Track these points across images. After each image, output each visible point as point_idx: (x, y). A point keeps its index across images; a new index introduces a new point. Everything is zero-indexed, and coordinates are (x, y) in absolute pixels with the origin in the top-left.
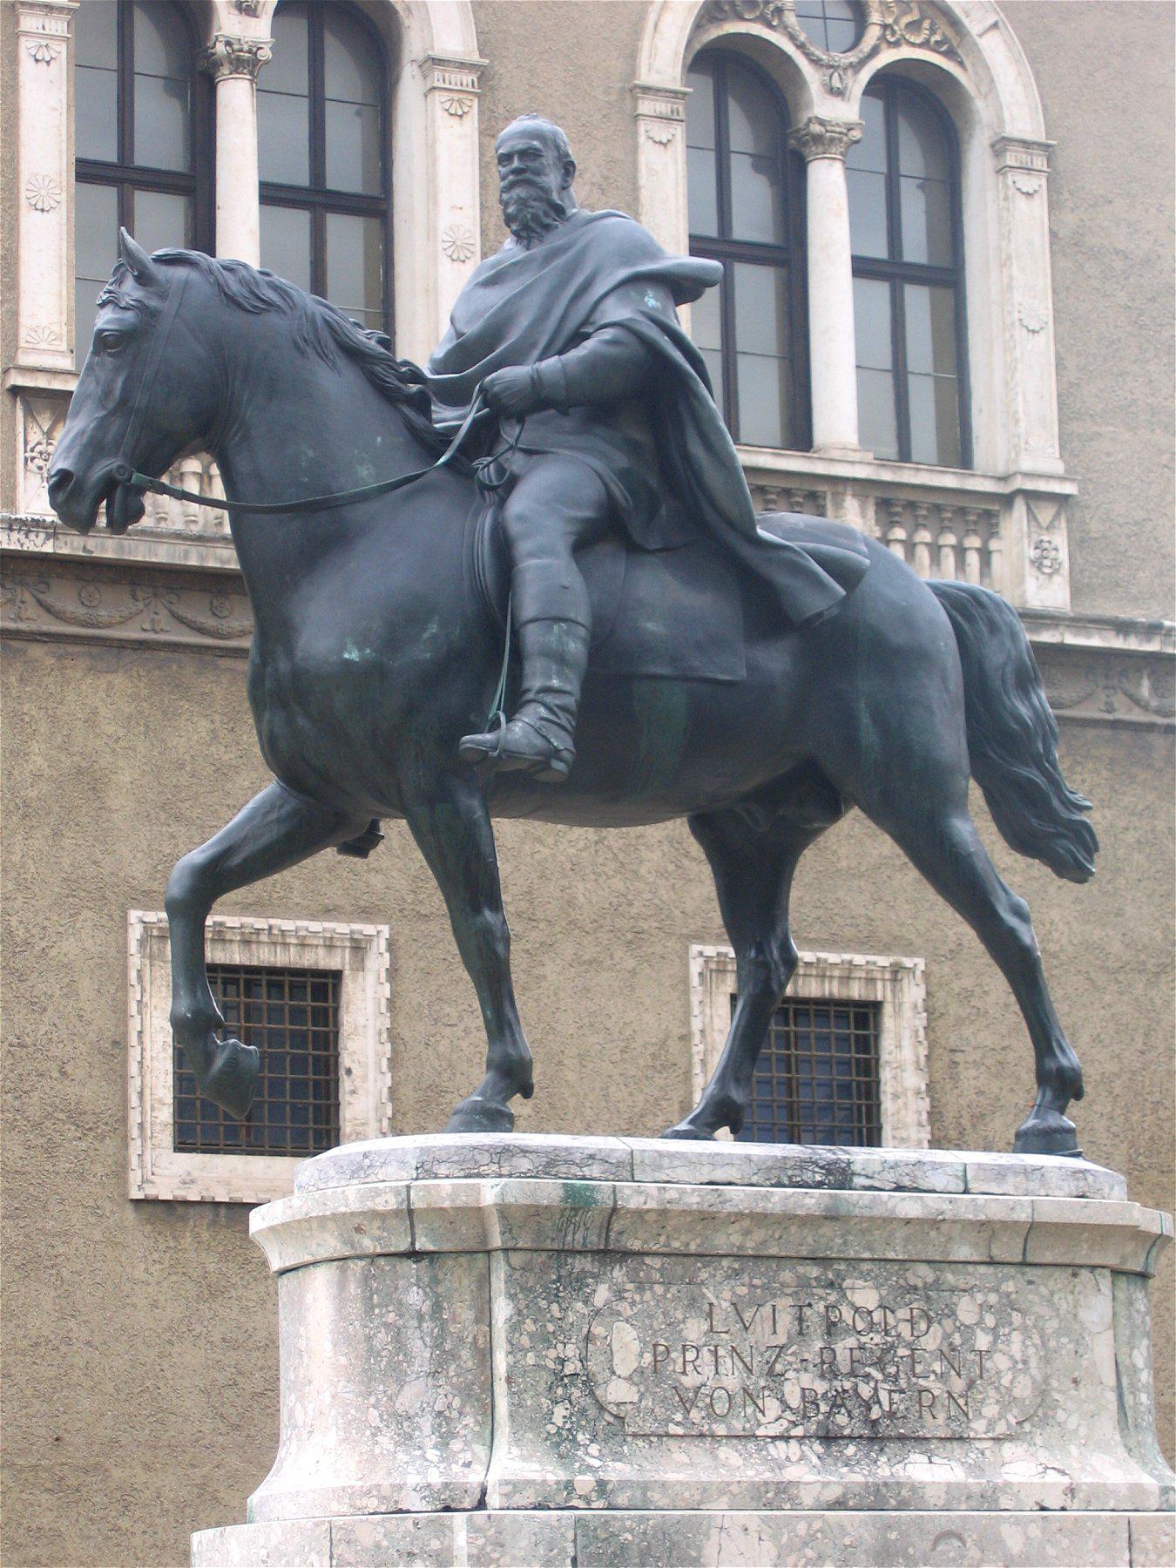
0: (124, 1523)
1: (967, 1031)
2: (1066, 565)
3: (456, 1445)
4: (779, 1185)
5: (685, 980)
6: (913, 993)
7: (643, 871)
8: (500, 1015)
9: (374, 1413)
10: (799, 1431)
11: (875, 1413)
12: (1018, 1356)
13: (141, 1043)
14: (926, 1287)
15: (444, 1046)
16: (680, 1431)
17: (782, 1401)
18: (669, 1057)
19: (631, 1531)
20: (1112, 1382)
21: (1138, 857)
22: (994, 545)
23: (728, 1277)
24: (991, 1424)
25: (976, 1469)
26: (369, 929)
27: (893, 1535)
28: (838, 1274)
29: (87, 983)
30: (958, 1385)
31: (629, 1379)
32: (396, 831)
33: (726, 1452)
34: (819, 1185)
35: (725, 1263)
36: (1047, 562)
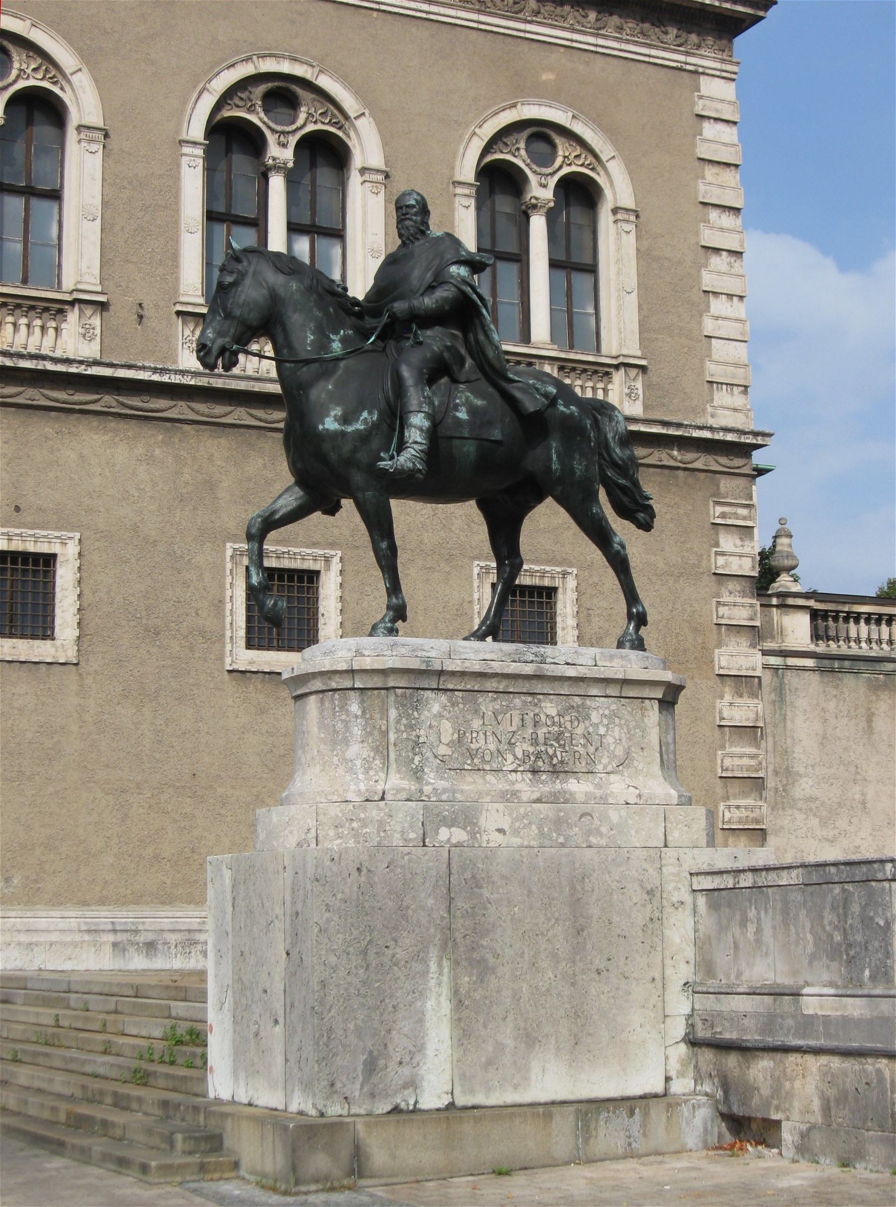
0: (223, 812)
1: (595, 601)
2: (641, 396)
3: (372, 773)
4: (514, 661)
5: (471, 577)
6: (571, 583)
7: (453, 528)
8: (394, 588)
9: (336, 759)
10: (521, 769)
11: (555, 761)
12: (617, 737)
13: (231, 601)
14: (578, 706)
15: (365, 604)
16: (470, 768)
17: (514, 755)
18: (462, 612)
19: (448, 811)
20: (658, 749)
21: (671, 525)
22: (610, 387)
23: (491, 701)
24: (605, 767)
25: (598, 786)
26: (333, 553)
27: (562, 814)
28: (539, 700)
29: (208, 574)
30: (591, 749)
31: (447, 745)
32: (347, 504)
33: (490, 777)
34: (532, 661)
35: (490, 694)
36: (633, 395)
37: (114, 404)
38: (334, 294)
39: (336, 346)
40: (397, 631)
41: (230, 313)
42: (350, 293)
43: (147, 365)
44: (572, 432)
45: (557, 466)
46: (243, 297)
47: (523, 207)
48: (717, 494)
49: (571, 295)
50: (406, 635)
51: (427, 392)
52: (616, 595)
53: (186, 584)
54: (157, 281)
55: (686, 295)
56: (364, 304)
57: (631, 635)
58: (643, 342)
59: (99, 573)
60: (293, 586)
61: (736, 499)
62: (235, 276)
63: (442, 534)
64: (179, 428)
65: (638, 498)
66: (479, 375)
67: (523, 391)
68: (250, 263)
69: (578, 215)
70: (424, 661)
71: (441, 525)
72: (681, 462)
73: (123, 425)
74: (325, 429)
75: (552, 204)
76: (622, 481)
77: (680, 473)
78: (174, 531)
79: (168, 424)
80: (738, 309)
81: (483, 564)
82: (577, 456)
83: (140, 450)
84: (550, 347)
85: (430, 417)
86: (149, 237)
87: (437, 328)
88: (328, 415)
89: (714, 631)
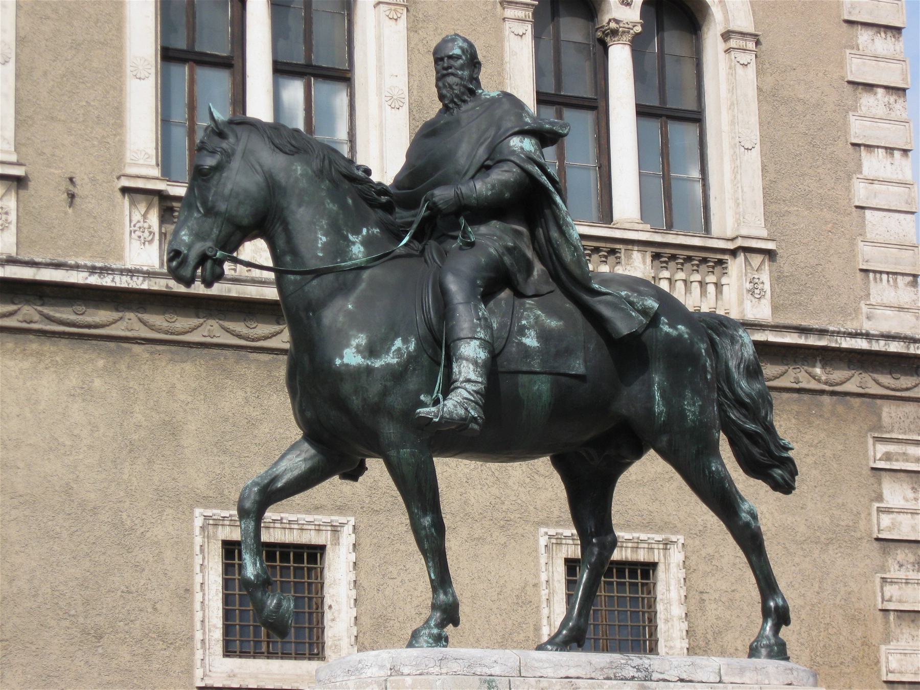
1: (710, 580)
5: (536, 550)
6: (676, 556)
7: (510, 482)
8: (442, 579)
13: (202, 589)
22: (724, 280)
26: (343, 520)
29: (169, 552)
32: (376, 467)
34: (633, 678)
36: (757, 291)
37: (37, 317)
38: (352, 179)
39: (358, 250)
40: (447, 640)
41: (213, 207)
42: (375, 178)
43: (81, 262)
44: (680, 358)
45: (662, 408)
46: (229, 186)
47: (599, 34)
48: (878, 427)
49: (668, 154)
50: (460, 644)
51: (483, 311)
52: (738, 572)
53: (138, 568)
54: (94, 146)
55: (829, 151)
56: (392, 191)
57: (767, 637)
58: (768, 217)
59: (17, 553)
60: (289, 568)
61: (905, 433)
62: (218, 157)
63: (495, 491)
64: (126, 349)
65: (773, 447)
66: (553, 286)
67: (614, 306)
68: (238, 139)
69: (675, 43)
70: (485, 681)
71: (492, 479)
72: (826, 383)
73: (48, 347)
74: (343, 365)
75: (638, 29)
76: (751, 426)
77: (826, 399)
78: (122, 494)
79: (112, 345)
80: (901, 168)
81: (552, 532)
82: (688, 394)
83: (73, 380)
84: (641, 227)
85: (487, 345)
86: (81, 86)
87: (494, 222)
88: (348, 345)
89: (879, 621)
